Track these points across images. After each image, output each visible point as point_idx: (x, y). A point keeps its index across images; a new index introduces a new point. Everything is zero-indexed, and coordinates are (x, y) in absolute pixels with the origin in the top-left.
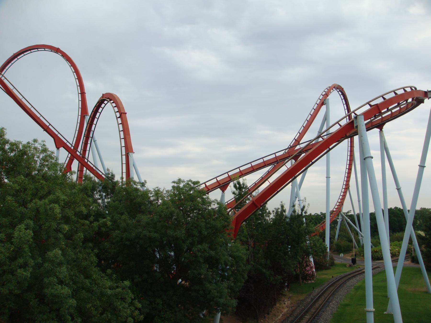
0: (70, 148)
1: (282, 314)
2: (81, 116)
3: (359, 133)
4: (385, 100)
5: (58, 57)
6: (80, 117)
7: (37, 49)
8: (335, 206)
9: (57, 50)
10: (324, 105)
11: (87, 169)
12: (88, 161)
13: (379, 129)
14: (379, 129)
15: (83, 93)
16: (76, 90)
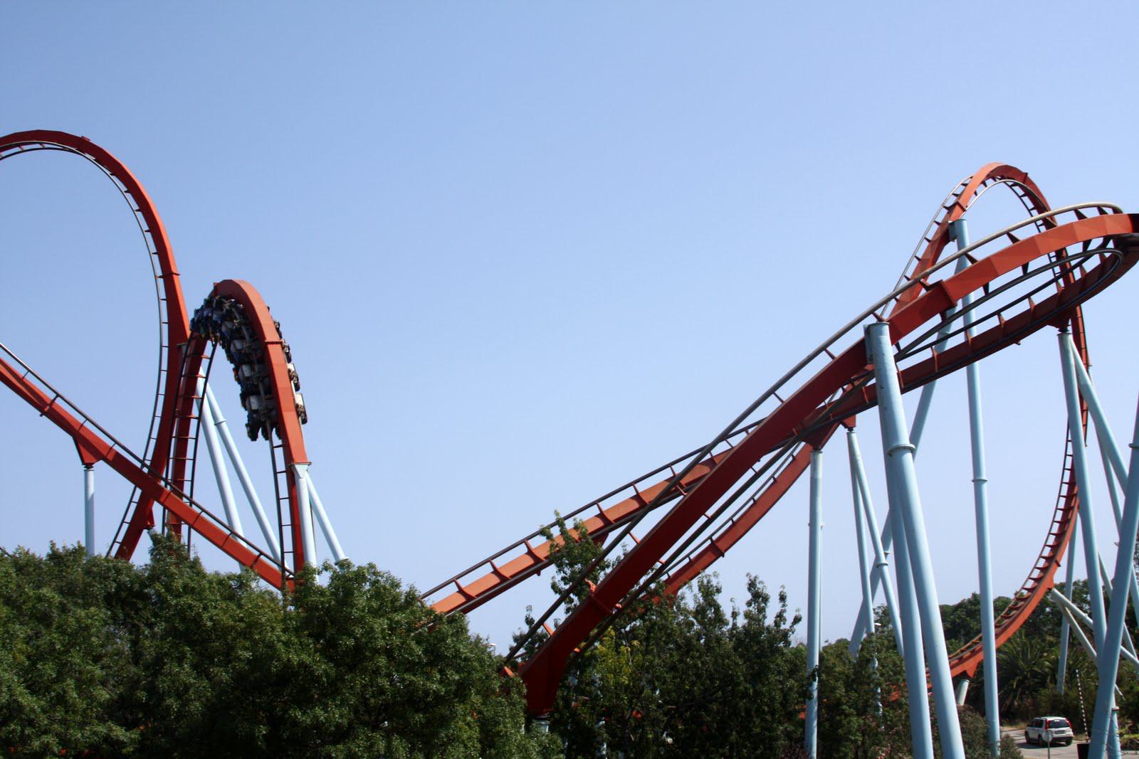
0: (140, 471)
1: (153, 595)
2: (170, 347)
3: (876, 374)
4: (975, 264)
5: (84, 164)
6: (165, 351)
7: (19, 145)
8: (1032, 571)
9: (81, 145)
10: (951, 243)
11: (191, 527)
12: (192, 503)
13: (1057, 327)
14: (1058, 329)
15: (168, 276)
16: (149, 267)
